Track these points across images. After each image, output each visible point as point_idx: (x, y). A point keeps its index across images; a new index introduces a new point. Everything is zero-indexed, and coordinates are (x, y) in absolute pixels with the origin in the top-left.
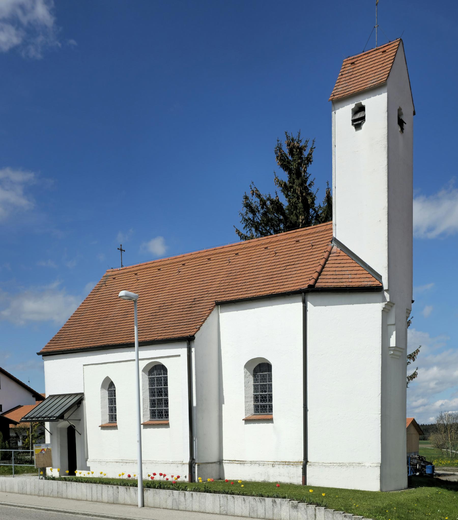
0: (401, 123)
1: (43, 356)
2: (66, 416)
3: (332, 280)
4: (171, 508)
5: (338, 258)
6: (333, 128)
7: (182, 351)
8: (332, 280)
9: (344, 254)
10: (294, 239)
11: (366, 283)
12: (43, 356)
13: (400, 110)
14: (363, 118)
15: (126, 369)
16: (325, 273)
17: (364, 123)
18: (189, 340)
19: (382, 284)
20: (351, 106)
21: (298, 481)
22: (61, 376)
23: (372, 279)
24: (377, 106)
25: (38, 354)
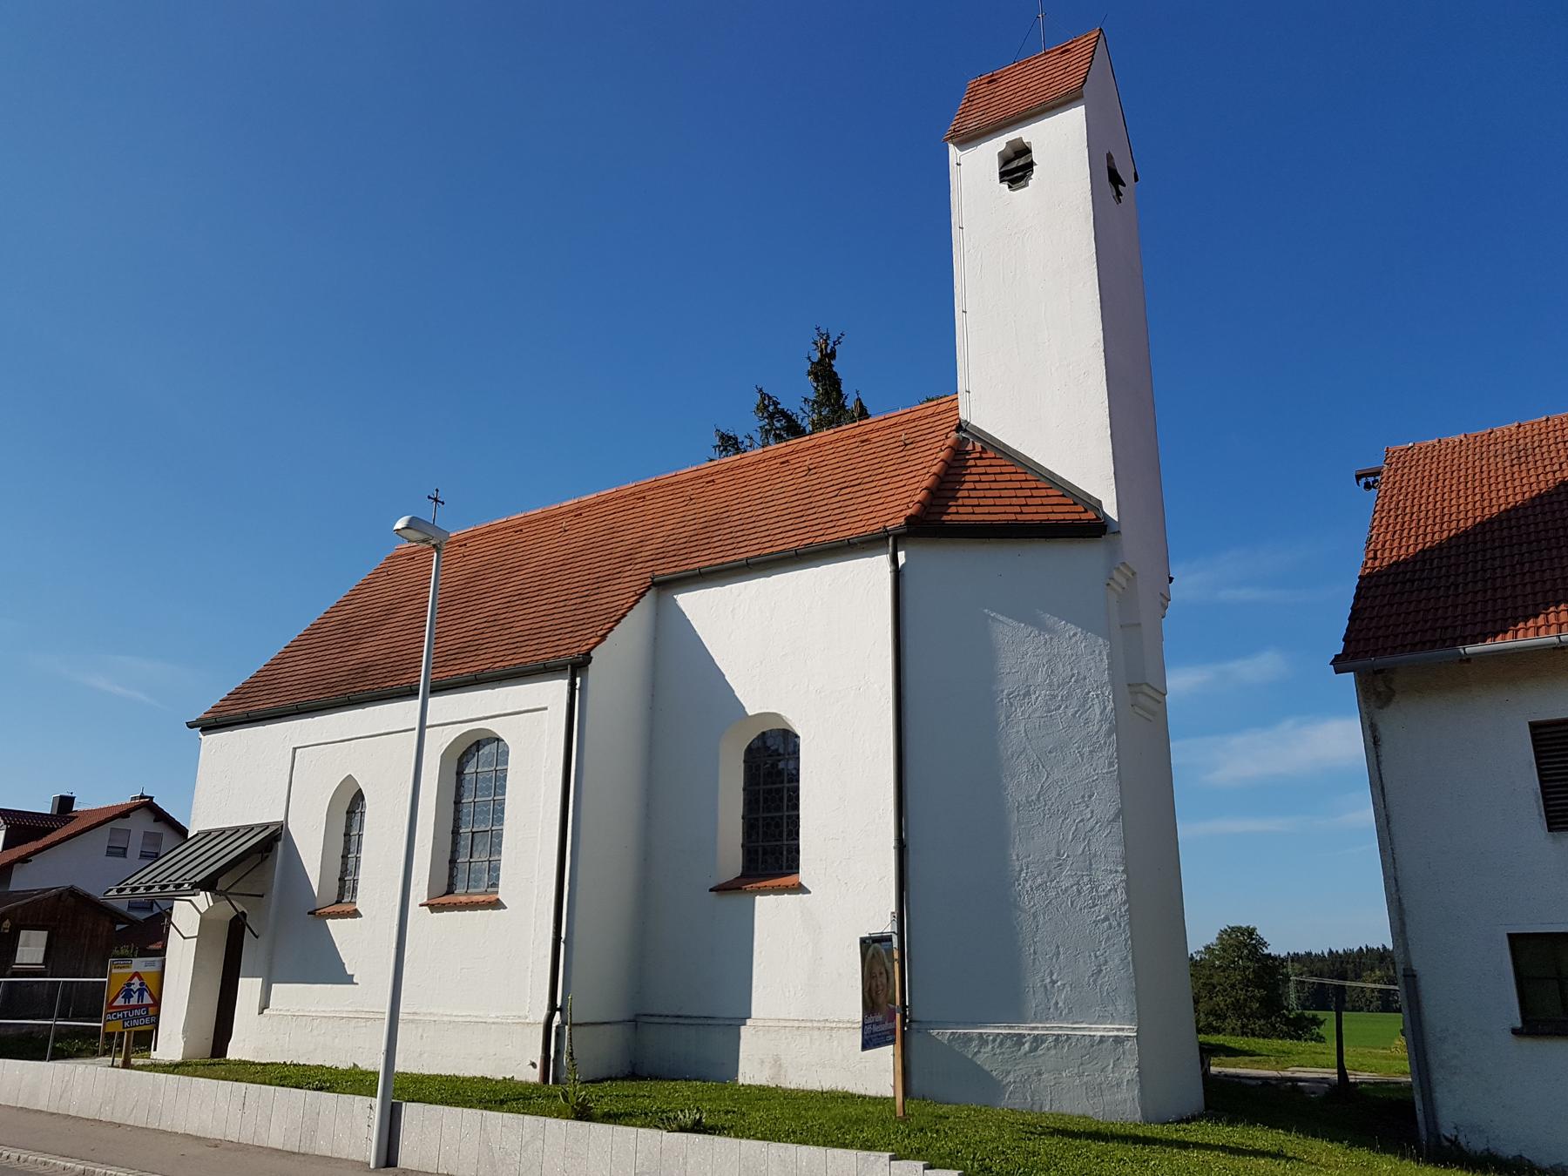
0: (1115, 179)
2: (222, 884)
7: (554, 691)
13: (1109, 157)
15: (381, 751)
18: (577, 667)
20: (999, 143)
24: (1061, 140)
25: (191, 725)
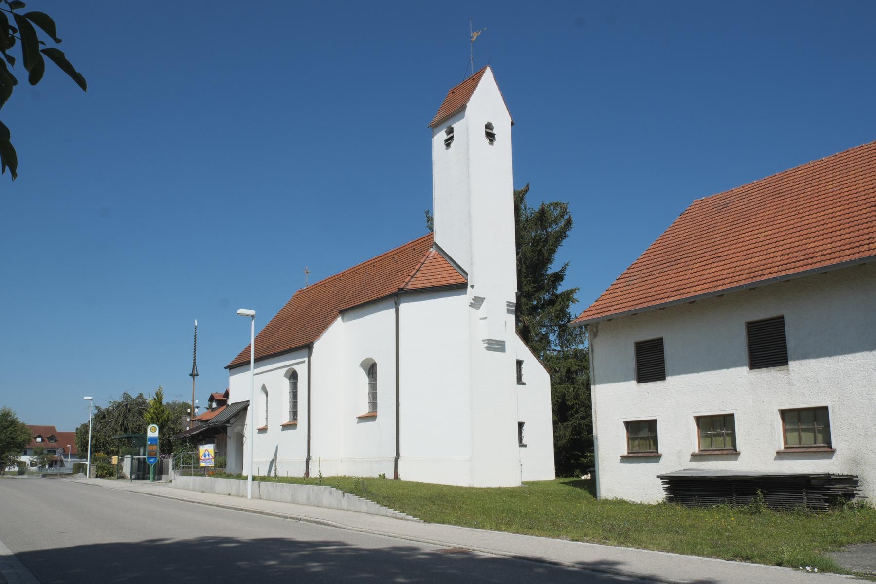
2: (231, 421)
14: (452, 138)
21: (390, 476)
25: (226, 368)
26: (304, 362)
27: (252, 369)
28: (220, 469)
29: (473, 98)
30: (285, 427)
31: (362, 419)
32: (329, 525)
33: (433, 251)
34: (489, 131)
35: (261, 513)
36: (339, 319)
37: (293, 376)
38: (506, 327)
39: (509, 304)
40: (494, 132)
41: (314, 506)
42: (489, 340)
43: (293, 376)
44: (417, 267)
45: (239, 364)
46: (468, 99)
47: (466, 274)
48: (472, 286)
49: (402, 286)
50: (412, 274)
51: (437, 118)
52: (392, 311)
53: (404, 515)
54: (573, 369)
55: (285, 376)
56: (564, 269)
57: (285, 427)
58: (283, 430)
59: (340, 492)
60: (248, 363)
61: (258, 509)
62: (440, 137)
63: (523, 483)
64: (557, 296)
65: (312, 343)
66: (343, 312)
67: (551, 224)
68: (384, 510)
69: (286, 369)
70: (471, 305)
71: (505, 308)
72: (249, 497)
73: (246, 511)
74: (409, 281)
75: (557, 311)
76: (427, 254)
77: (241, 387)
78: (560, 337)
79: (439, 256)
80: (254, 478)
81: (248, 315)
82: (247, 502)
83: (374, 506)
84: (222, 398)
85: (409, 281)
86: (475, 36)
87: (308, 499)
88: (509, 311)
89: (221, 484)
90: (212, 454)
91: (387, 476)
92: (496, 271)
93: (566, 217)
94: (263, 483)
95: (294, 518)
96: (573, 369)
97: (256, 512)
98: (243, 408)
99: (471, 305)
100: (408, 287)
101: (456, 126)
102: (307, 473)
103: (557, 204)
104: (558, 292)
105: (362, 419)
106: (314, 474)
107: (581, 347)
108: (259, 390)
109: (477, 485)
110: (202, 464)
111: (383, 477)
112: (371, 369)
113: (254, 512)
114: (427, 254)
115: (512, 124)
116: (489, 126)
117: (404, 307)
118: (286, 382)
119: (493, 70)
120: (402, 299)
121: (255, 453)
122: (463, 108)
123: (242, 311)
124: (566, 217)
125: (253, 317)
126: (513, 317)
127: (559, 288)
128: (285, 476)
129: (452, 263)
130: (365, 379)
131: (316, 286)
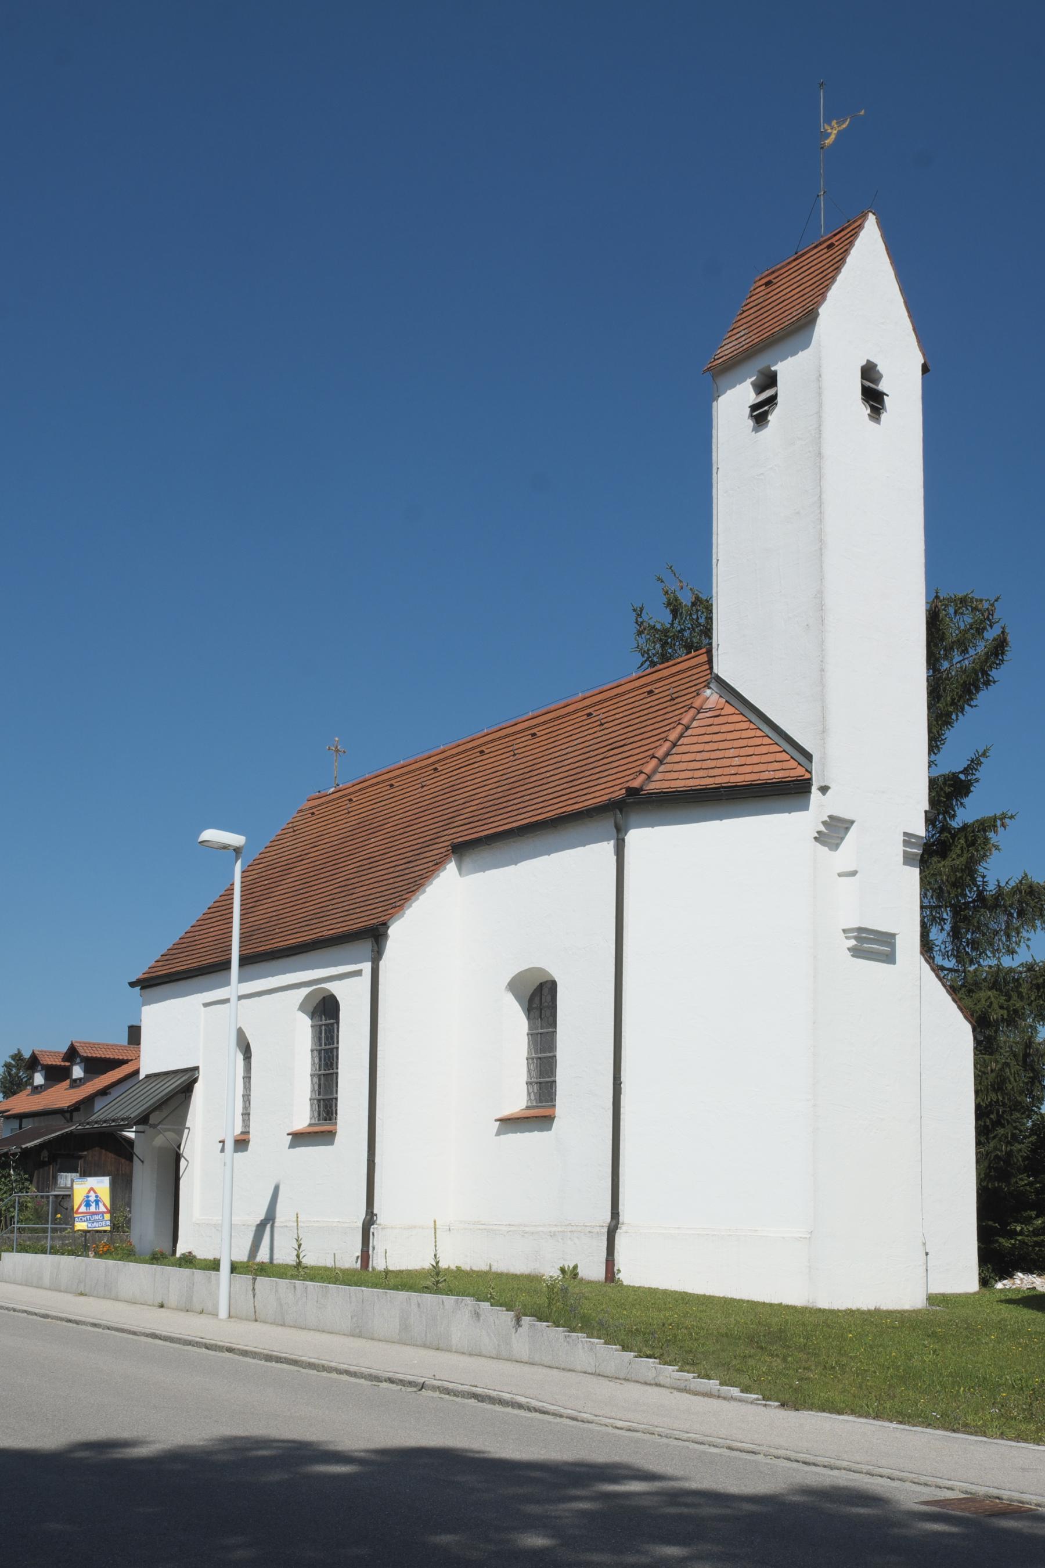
1: (142, 988)
2: (153, 1119)
3: (689, 774)
4: (494, 1353)
5: (717, 720)
6: (714, 432)
8: (689, 774)
9: (732, 710)
10: (645, 690)
11: (772, 775)
12: (142, 988)
14: (772, 400)
15: (270, 1010)
16: (676, 758)
17: (774, 409)
19: (810, 773)
21: (593, 1270)
22: (175, 1033)
23: (785, 765)
25: (132, 985)
26: (359, 973)
27: (235, 985)
28: (114, 1243)
29: (834, 293)
30: (299, 1138)
31: (510, 1123)
32: (529, 1409)
33: (711, 696)
34: (868, 384)
35: (295, 1362)
36: (451, 867)
37: (325, 1010)
38: (898, 900)
39: (909, 839)
40: (882, 387)
41: (425, 1346)
42: (860, 930)
43: (325, 1010)
44: (673, 736)
45: (156, 982)
46: (823, 296)
47: (809, 757)
48: (824, 789)
49: (636, 784)
50: (660, 753)
51: (728, 349)
52: (608, 847)
53: (713, 1384)
54: (994, 1016)
55: (302, 1008)
56: (974, 765)
57: (299, 1138)
58: (292, 1145)
59: (506, 1317)
60: (226, 965)
61: (276, 1350)
62: (735, 400)
63: (932, 1299)
64: (955, 834)
65: (385, 925)
66: (461, 850)
67: (949, 649)
68: (648, 1367)
69: (305, 991)
70: (820, 838)
71: (897, 850)
72: (223, 1313)
73: (245, 1353)
74: (655, 771)
75: (954, 869)
76: (697, 703)
77: (175, 1033)
78: (956, 934)
79: (729, 710)
80: (234, 1268)
81: (225, 847)
82: (220, 1328)
83: (613, 1357)
84: (58, 1062)
85: (655, 771)
86: (833, 131)
87: (405, 1327)
88: (908, 859)
89: (135, 1277)
90: (108, 1202)
91: (582, 1273)
92: (878, 757)
93: (991, 634)
94: (262, 1281)
95: (402, 1382)
96: (994, 1016)
97: (279, 1360)
98: (181, 1087)
99: (820, 838)
100: (653, 787)
101: (786, 369)
102: (365, 1257)
103: (963, 601)
104: (956, 824)
105: (510, 1123)
106: (378, 1263)
107: (1007, 962)
108: (223, 1043)
109: (824, 1304)
110: (80, 1226)
111: (571, 1274)
112: (540, 999)
113: (269, 1358)
114: (697, 703)
115: (925, 369)
116: (869, 372)
117: (637, 838)
118: (304, 1028)
119: (882, 225)
120: (633, 818)
121: (213, 1204)
122: (807, 320)
123: (210, 835)
124: (991, 634)
125: (237, 851)
126: (916, 871)
127: (960, 812)
128: (329, 1263)
129: (767, 730)
130: (516, 1023)
131: (363, 786)
